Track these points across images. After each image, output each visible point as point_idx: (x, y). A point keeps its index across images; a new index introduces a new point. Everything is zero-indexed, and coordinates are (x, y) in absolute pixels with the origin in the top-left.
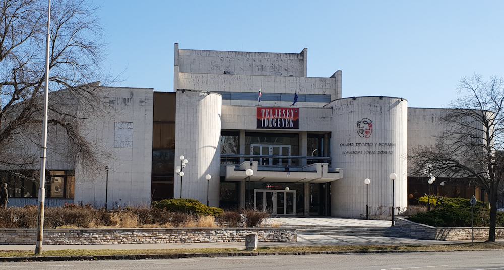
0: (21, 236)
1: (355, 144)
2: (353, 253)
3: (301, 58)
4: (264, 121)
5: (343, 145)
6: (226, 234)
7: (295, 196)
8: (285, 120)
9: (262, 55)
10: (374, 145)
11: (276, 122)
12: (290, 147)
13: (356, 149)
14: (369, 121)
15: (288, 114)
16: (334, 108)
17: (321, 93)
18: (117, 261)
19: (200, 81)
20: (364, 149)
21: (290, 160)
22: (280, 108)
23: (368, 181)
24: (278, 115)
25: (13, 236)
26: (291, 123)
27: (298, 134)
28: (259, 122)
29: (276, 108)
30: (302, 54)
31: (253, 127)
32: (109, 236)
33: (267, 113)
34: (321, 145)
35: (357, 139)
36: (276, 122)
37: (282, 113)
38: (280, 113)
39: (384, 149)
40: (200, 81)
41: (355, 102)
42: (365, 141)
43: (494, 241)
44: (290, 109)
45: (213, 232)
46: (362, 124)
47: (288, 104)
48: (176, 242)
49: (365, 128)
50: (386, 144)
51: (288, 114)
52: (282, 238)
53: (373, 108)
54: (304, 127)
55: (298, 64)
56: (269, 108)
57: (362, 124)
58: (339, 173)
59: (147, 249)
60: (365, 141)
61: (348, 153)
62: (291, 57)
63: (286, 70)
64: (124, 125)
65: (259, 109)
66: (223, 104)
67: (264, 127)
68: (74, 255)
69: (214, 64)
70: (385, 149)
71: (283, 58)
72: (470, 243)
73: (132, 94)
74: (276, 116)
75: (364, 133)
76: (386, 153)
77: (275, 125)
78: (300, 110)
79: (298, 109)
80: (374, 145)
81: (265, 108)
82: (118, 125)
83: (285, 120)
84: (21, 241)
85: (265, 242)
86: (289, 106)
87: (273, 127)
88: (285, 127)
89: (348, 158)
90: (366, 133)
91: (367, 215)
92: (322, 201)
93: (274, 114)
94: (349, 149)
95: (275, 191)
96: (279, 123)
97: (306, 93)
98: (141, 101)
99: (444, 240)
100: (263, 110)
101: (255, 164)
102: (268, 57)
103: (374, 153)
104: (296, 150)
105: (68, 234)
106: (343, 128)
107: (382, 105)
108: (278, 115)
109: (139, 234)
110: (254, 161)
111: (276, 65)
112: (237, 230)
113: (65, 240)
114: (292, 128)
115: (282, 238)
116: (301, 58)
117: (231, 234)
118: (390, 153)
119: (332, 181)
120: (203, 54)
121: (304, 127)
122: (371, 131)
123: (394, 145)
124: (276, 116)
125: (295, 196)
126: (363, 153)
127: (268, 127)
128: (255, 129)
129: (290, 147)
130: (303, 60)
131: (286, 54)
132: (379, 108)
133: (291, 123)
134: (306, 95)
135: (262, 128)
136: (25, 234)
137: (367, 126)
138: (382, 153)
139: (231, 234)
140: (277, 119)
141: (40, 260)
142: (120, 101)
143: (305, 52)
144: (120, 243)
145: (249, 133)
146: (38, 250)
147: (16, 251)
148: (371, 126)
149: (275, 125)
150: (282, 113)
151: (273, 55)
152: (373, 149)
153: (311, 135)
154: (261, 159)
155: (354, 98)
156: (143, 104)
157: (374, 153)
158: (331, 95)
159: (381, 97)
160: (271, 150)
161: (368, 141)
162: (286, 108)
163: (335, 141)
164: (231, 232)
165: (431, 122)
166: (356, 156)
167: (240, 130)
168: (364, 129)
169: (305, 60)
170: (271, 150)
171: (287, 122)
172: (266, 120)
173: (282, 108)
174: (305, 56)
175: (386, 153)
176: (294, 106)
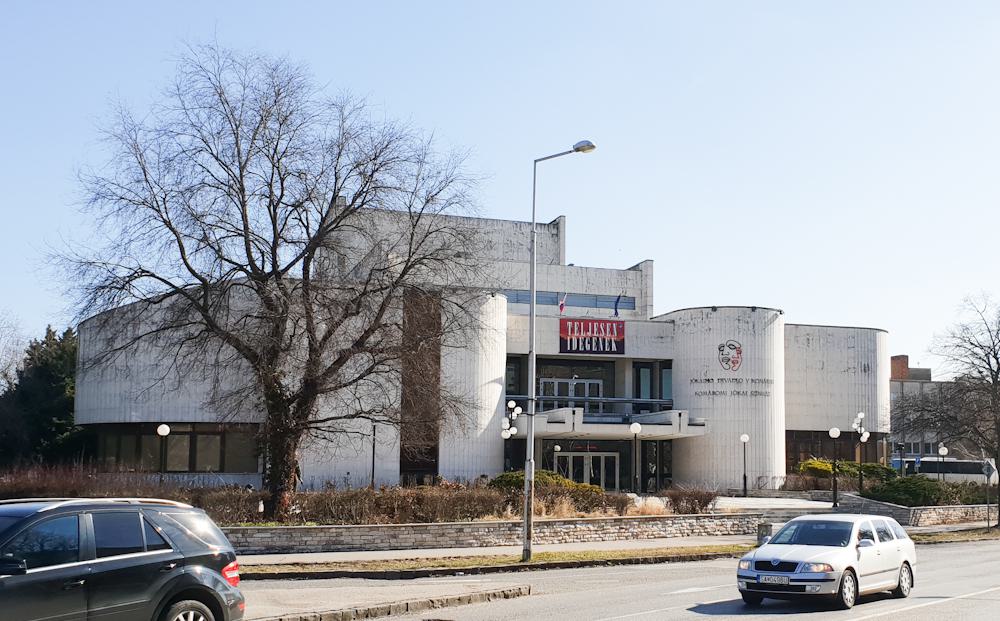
0: (435, 535)
1: (716, 381)
3: (554, 231)
4: (571, 340)
6: (685, 524)
7: (617, 462)
8: (604, 340)
9: (490, 223)
10: (745, 381)
11: (590, 343)
12: (600, 382)
13: (718, 387)
14: (737, 345)
15: (608, 330)
16: (678, 322)
18: (652, 566)
20: (730, 387)
21: (601, 405)
22: (596, 321)
23: (745, 438)
24: (593, 332)
25: (424, 536)
26: (614, 345)
27: (613, 362)
28: (563, 342)
29: (590, 321)
30: (556, 224)
31: (553, 349)
32: (547, 531)
33: (576, 329)
34: (654, 382)
35: (717, 372)
36: (590, 343)
37: (599, 329)
38: (595, 330)
39: (760, 388)
42: (730, 375)
44: (612, 322)
45: (669, 522)
47: (607, 313)
48: (627, 538)
49: (730, 356)
50: (761, 381)
51: (608, 330)
52: (748, 528)
54: (631, 352)
55: (550, 242)
56: (580, 321)
58: (704, 425)
59: (597, 550)
60: (730, 375)
61: (705, 393)
65: (563, 323)
66: (509, 311)
67: (571, 351)
68: (635, 556)
70: (759, 389)
72: (984, 528)
74: (589, 334)
75: (730, 363)
76: (761, 394)
77: (588, 347)
78: (626, 323)
79: (623, 322)
80: (745, 381)
81: (573, 321)
83: (604, 340)
84: (435, 544)
85: (729, 534)
86: (607, 317)
87: (585, 351)
88: (604, 352)
89: (704, 401)
91: (745, 489)
92: (656, 468)
93: (586, 330)
94: (706, 387)
95: (570, 455)
96: (594, 344)
97: (597, 293)
99: (917, 525)
100: (570, 324)
101: (580, 411)
103: (745, 393)
104: (611, 390)
105: (492, 529)
106: (694, 356)
107: (754, 317)
108: (593, 332)
109: (583, 527)
110: (576, 406)
111: (514, 241)
112: (698, 518)
113: (492, 539)
114: (614, 353)
115: (748, 528)
117: (691, 525)
118: (766, 394)
119: (682, 439)
121: (631, 352)
122: (740, 360)
123: (772, 382)
124: (589, 334)
125: (617, 462)
126: (729, 393)
127: (577, 351)
129: (600, 382)
130: (557, 235)
132: (751, 325)
133: (614, 345)
134: (596, 296)
135: (569, 352)
136: (441, 532)
137: (733, 353)
138: (755, 394)
139: (691, 525)
140: (591, 338)
141: (533, 567)
143: (561, 223)
144: (560, 542)
145: (542, 361)
146: (527, 552)
148: (740, 352)
149: (588, 347)
150: (599, 329)
152: (744, 387)
153: (639, 365)
154: (587, 404)
155: (714, 309)
157: (745, 393)
158: (634, 298)
159: (754, 309)
160: (571, 388)
161: (736, 375)
162: (605, 322)
163: (680, 374)
164: (690, 521)
165: (805, 346)
166: (718, 399)
168: (730, 356)
169: (561, 235)
170: (571, 388)
171: (607, 344)
172: (574, 338)
173: (600, 321)
174: (561, 229)
175: (761, 394)
176: (616, 319)
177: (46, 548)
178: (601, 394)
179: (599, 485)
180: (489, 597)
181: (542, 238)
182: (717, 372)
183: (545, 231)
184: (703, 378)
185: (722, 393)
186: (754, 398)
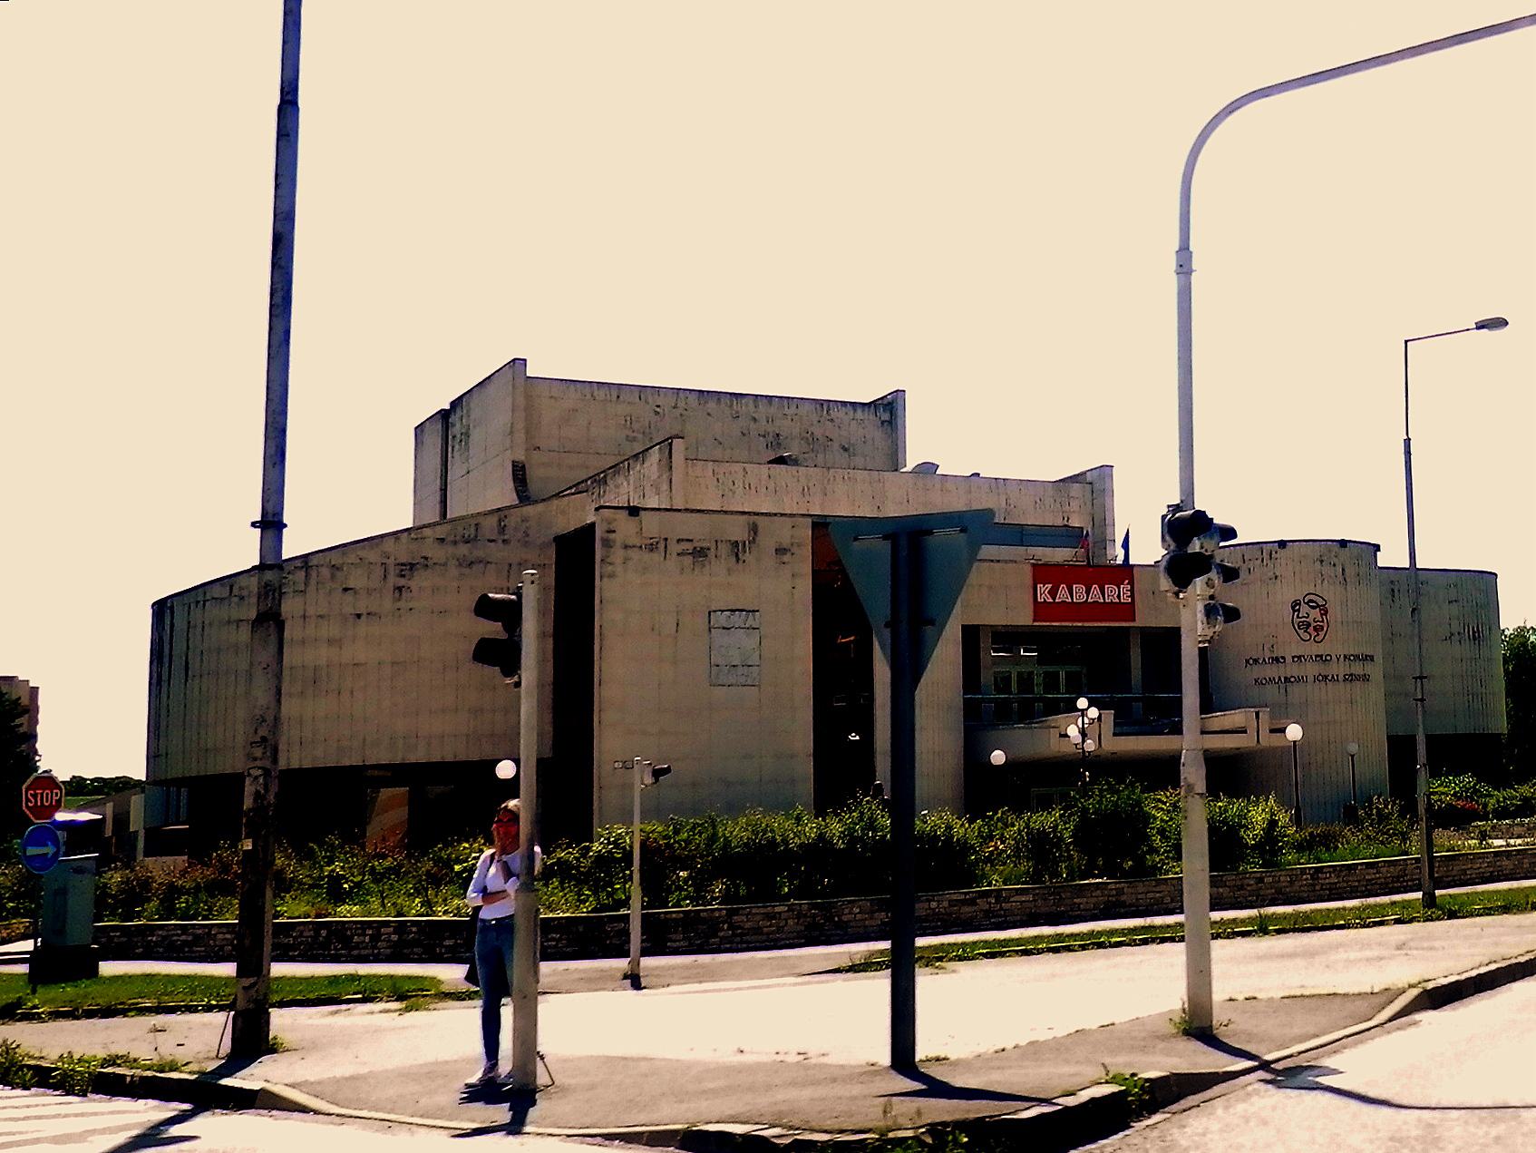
1: (1289, 659)
2: (986, 956)
3: (886, 417)
5: (1256, 661)
13: (1293, 670)
14: (1321, 602)
17: (1059, 522)
19: (739, 483)
20: (1311, 669)
40: (739, 483)
41: (1282, 553)
43: (93, 973)
46: (1304, 609)
53: (1327, 570)
57: (1304, 609)
62: (859, 414)
63: (846, 450)
64: (737, 619)
69: (636, 426)
71: (834, 414)
73: (754, 529)
75: (1311, 630)
82: (720, 619)
90: (1315, 629)
98: (781, 551)
102: (773, 410)
111: (818, 432)
116: (886, 417)
120: (600, 394)
128: (1030, 623)
130: (890, 422)
131: (844, 403)
137: (1315, 614)
142: (724, 549)
143: (900, 402)
147: (1410, 921)
151: (807, 406)
155: (1282, 544)
156: (786, 558)
167: (978, 626)
168: (1310, 620)
177: (450, 1035)
178: (1062, 688)
179: (1430, 805)
180: (112, 1113)
181: (870, 429)
182: (1292, 645)
183: (869, 416)
184: (1268, 655)
185: (1298, 680)
186: (1348, 685)
